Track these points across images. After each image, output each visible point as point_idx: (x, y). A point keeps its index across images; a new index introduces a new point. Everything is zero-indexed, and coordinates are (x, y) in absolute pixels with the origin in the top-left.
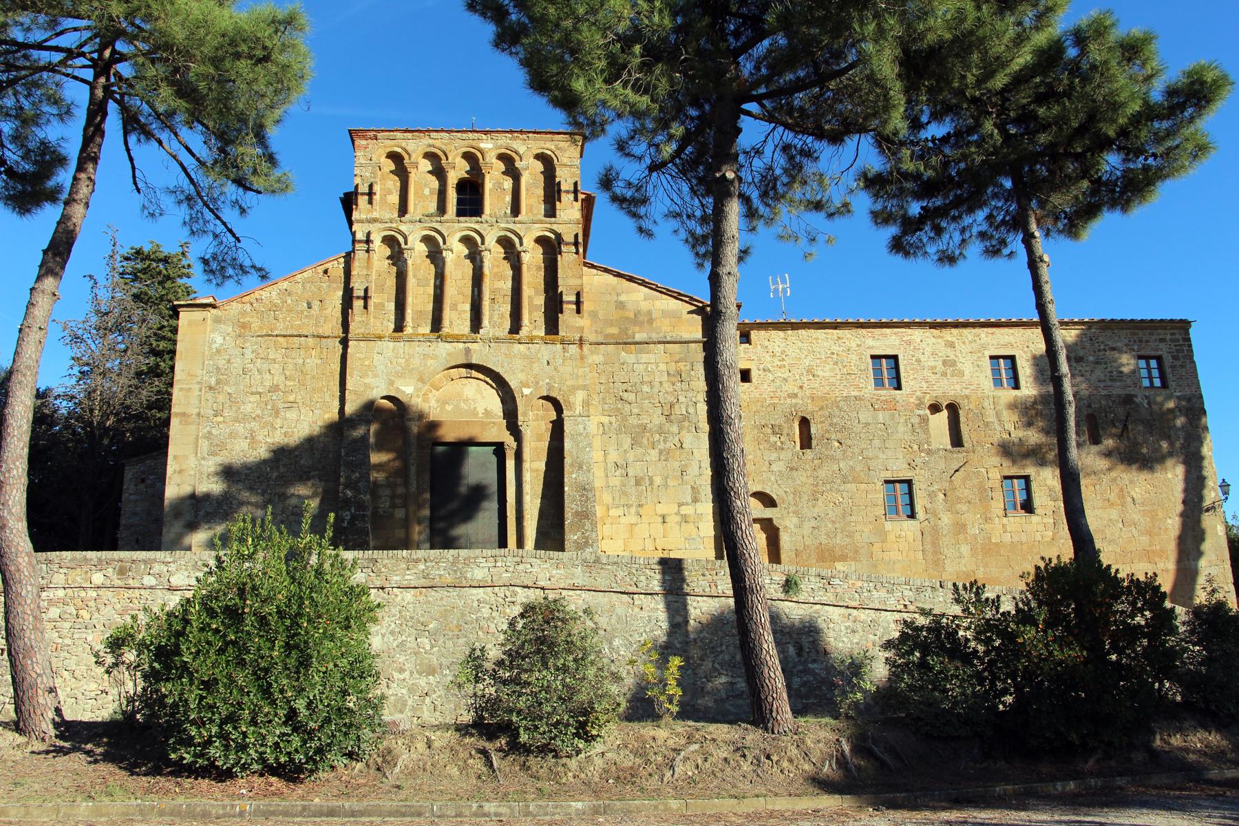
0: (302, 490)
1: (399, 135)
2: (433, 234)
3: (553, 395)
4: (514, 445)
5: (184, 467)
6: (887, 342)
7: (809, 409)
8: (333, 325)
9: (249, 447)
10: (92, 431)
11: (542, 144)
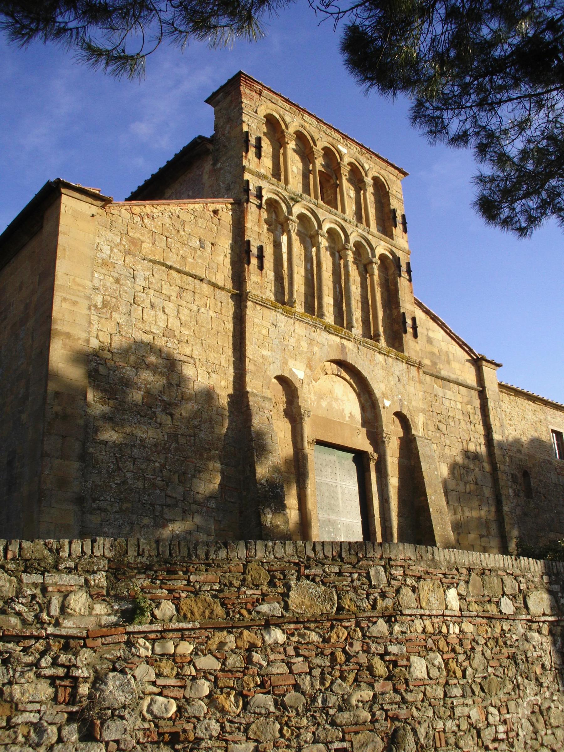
1: (281, 102)
2: (309, 214)
3: (405, 412)
4: (376, 456)
8: (223, 275)
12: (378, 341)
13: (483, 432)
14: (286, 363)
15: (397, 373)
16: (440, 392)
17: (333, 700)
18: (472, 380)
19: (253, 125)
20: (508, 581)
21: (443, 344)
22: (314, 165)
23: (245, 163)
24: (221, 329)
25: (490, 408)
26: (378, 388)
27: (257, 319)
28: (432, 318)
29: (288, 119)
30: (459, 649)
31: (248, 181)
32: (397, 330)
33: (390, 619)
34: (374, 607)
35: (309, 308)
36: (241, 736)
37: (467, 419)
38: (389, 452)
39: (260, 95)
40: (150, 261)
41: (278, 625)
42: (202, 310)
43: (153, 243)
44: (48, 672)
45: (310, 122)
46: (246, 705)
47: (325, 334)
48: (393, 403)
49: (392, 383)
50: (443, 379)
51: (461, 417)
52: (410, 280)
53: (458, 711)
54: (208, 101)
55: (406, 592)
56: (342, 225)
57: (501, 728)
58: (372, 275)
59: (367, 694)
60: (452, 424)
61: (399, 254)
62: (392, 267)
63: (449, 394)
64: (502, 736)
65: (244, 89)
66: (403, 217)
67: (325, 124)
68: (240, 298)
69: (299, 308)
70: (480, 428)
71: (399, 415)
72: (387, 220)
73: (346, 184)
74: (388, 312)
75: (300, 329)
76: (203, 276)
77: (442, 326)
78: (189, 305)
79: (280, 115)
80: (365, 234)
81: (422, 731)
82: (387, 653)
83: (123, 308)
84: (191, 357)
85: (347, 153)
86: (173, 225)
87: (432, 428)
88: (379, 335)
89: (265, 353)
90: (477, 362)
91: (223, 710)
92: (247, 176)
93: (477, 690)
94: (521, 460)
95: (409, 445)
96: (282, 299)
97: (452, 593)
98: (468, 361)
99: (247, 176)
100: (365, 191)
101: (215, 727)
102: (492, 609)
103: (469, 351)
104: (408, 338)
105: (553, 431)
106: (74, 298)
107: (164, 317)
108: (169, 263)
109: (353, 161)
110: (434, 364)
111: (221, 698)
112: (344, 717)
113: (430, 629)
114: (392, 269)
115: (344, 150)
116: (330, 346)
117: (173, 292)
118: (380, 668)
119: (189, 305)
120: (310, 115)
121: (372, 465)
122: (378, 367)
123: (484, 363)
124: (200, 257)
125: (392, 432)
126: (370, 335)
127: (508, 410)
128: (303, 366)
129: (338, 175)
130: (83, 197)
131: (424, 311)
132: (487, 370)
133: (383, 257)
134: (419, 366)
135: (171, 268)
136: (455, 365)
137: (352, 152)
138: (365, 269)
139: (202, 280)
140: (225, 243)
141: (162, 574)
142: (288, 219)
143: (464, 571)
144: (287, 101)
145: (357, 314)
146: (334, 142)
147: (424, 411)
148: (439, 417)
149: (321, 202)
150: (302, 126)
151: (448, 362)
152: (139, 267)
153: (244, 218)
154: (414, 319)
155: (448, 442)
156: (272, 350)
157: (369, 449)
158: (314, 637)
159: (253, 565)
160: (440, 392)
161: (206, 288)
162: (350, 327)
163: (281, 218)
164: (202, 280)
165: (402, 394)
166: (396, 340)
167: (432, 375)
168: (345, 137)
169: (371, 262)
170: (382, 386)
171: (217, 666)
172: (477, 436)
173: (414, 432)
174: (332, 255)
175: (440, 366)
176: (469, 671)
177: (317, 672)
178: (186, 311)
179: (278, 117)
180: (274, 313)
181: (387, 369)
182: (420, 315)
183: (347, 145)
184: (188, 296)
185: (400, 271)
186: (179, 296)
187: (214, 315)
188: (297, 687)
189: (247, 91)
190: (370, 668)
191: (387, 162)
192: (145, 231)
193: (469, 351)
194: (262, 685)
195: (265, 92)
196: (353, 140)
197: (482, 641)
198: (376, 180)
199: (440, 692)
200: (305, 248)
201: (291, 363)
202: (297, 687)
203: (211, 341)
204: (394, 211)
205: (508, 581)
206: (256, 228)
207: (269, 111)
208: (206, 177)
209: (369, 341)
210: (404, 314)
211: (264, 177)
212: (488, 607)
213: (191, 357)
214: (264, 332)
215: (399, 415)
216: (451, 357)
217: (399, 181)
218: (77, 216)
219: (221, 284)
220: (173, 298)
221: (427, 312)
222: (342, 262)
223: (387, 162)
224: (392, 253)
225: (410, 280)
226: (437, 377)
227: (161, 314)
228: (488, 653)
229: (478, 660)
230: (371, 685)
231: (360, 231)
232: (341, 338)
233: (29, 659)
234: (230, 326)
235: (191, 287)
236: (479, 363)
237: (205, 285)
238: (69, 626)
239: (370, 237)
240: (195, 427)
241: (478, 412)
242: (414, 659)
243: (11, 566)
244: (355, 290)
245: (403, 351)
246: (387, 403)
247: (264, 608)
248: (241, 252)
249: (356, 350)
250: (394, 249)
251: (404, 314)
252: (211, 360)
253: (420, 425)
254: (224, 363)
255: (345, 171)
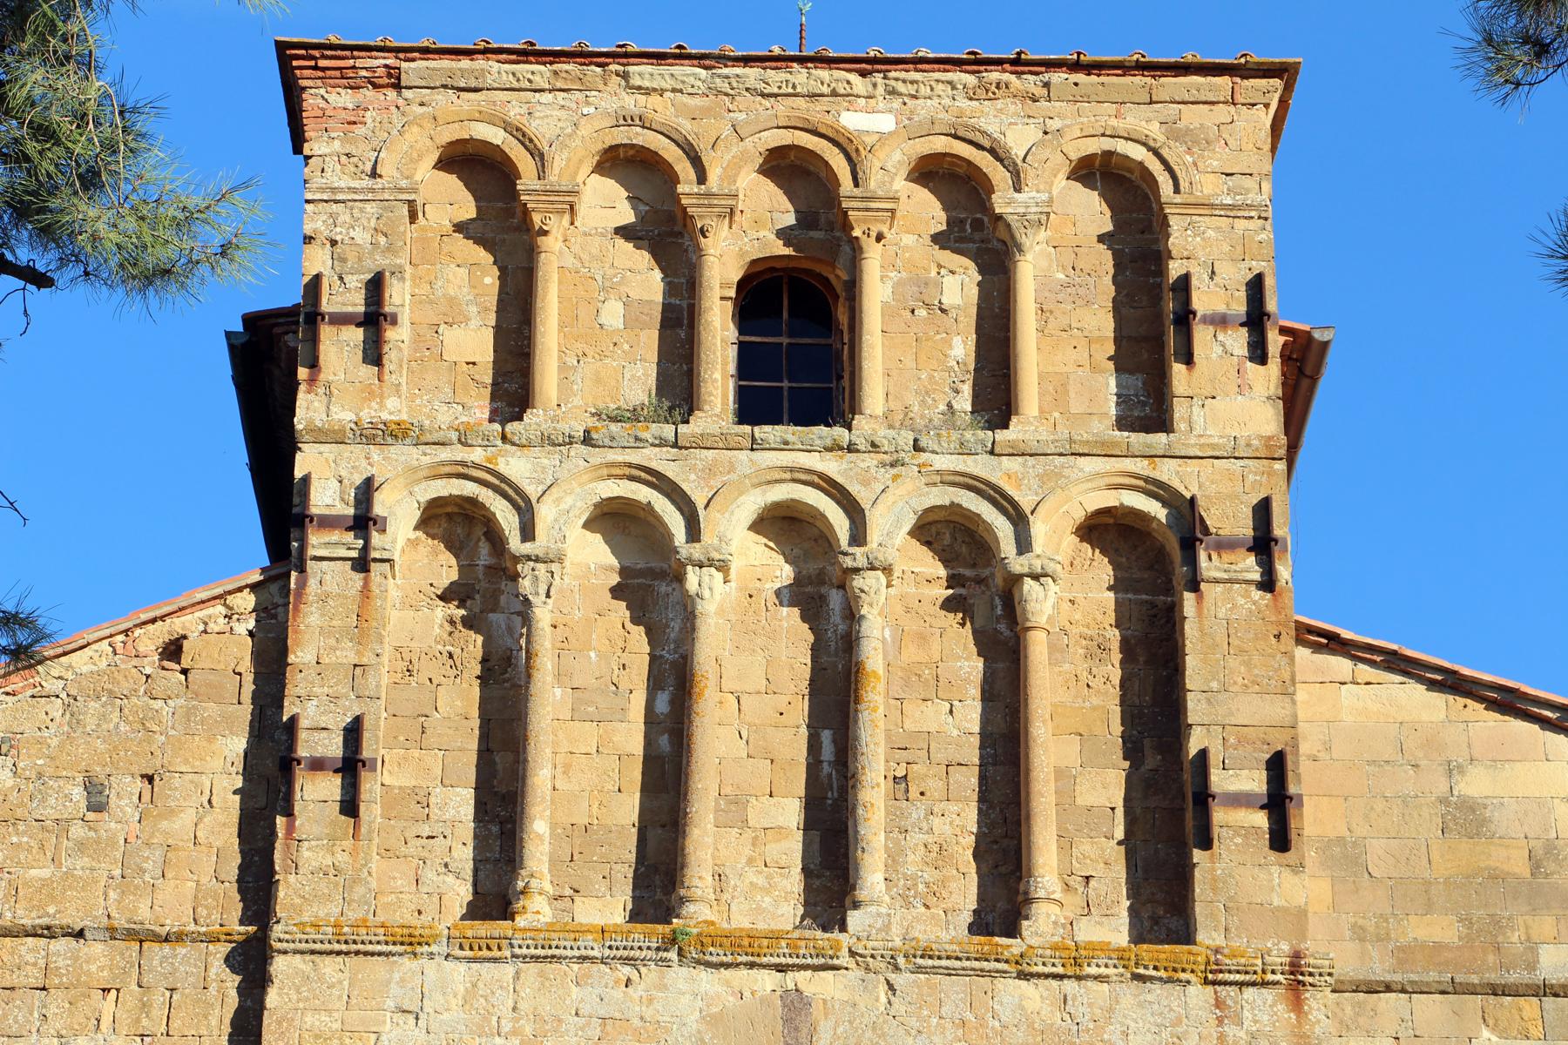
1: (495, 70)
2: (643, 494)
28: (1493, 705)
39: (397, 86)
45: (668, 84)
56: (822, 476)
67: (747, 61)
74: (1152, 761)
79: (508, 127)
131: (1433, 685)
139: (80, 934)
144: (527, 54)
180: (406, 962)
183: (893, 92)
195: (412, 70)
196: (918, 62)
207: (449, 134)
224: (1157, 489)
232: (781, 968)
237: (98, 948)
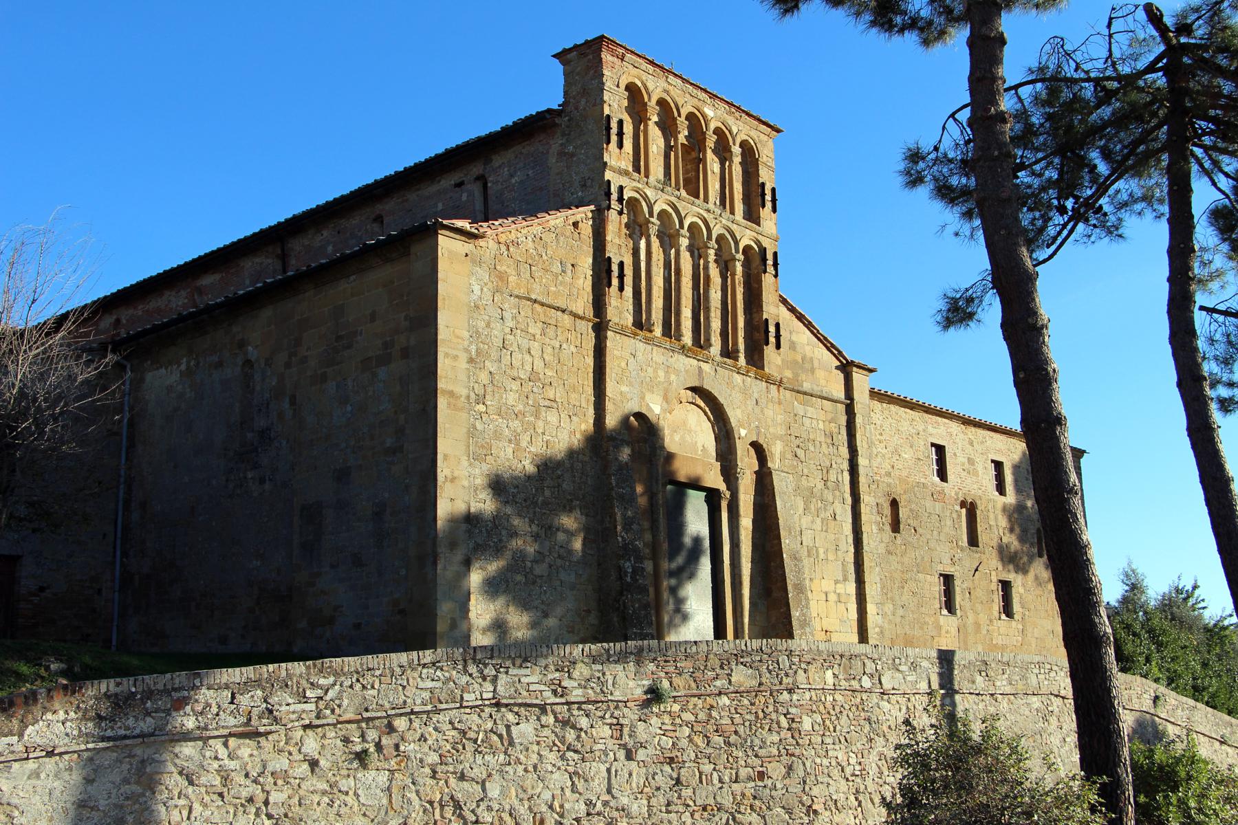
0: (568, 521)
1: (644, 65)
2: (670, 210)
3: (761, 441)
4: (728, 494)
5: (456, 474)
6: (943, 431)
7: (898, 492)
8: (583, 304)
9: (519, 457)
10: (125, 358)
11: (753, 133)
12: (736, 359)
13: (848, 456)
14: (643, 398)
15: (756, 395)
16: (800, 409)
17: (757, 742)
18: (841, 395)
19: (615, 104)
20: (869, 664)
21: (808, 348)
22: (676, 140)
23: (606, 158)
24: (581, 365)
25: (858, 426)
26: (735, 415)
27: (614, 342)
29: (651, 86)
30: (832, 712)
31: (609, 182)
32: (759, 337)
33: (790, 691)
34: (781, 683)
35: (667, 332)
36: (707, 761)
37: (829, 441)
38: (742, 489)
40: (517, 297)
41: (726, 694)
42: (564, 346)
43: (519, 275)
44: (609, 721)
46: (709, 742)
47: (682, 358)
48: (750, 432)
49: (750, 408)
50: (805, 393)
51: (823, 439)
52: (776, 276)
53: (830, 753)
54: (561, 56)
55: (801, 672)
57: (858, 767)
58: (733, 275)
59: (776, 738)
60: (812, 448)
61: (766, 243)
62: (757, 261)
63: (811, 411)
64: (857, 773)
65: (606, 56)
66: (773, 190)
67: (692, 84)
68: (600, 328)
69: (658, 331)
70: (844, 451)
71: (757, 447)
72: (756, 199)
73: (710, 155)
75: (658, 355)
76: (564, 307)
77: (809, 325)
78: (552, 342)
80: (730, 224)
81: (808, 764)
82: (788, 713)
83: (494, 354)
84: (555, 401)
85: (714, 114)
86: (536, 249)
87: (789, 456)
88: (738, 351)
89: (624, 388)
90: (846, 367)
91: (697, 746)
92: (608, 175)
93: (843, 740)
94: (889, 485)
95: (764, 480)
96: (641, 324)
97: (829, 673)
98: (837, 368)
99: (608, 175)
100: (731, 161)
101: (693, 756)
102: (855, 684)
103: (838, 354)
104: (769, 350)
105: (933, 445)
106: (455, 352)
107: (530, 360)
108: (533, 297)
109: (720, 125)
110: (796, 375)
111: (696, 738)
112: (762, 752)
113: (814, 698)
114: (757, 261)
115: (709, 112)
116: (687, 371)
117: (535, 329)
118: (784, 722)
119: (552, 342)
120: (676, 75)
121: (724, 504)
122: (738, 391)
123: (855, 369)
124: (561, 283)
125: (747, 464)
126: (729, 353)
127: (878, 423)
128: (659, 399)
129: (701, 147)
130: (458, 237)
132: (857, 376)
133: (747, 249)
134: (780, 384)
135: (535, 301)
136: (820, 374)
137: (719, 113)
138: (725, 267)
140: (586, 262)
141: (662, 663)
142: (649, 222)
143: (837, 657)
144: (652, 63)
145: (716, 324)
146: (699, 104)
147: (780, 438)
148: (797, 442)
149: (683, 193)
150: (666, 91)
151: (813, 370)
152: (506, 306)
153: (604, 228)
154: (777, 326)
155: (806, 471)
156: (631, 384)
157: (722, 487)
158: (746, 702)
159: (711, 656)
160: (800, 409)
161: (567, 320)
162: (708, 344)
163: (641, 220)
164: (563, 311)
165: (759, 420)
166: (755, 358)
167: (793, 390)
168: (713, 96)
169: (734, 259)
170: (738, 412)
171: (693, 718)
172: (839, 461)
173: (770, 464)
174: (692, 256)
175: (803, 377)
176: (838, 728)
177: (747, 724)
178: (549, 350)
179: (640, 84)
181: (745, 391)
182: (784, 315)
184: (551, 331)
185: (765, 265)
186: (543, 334)
187: (574, 350)
188: (736, 732)
189: (610, 58)
190: (778, 723)
191: (759, 120)
192: (510, 261)
193: (838, 354)
194: (717, 731)
197: (847, 707)
198: (744, 144)
199: (819, 739)
200: (664, 251)
201: (648, 397)
202: (736, 732)
203: (573, 380)
204: (763, 185)
205: (869, 664)
206: (617, 241)
208: (552, 160)
209: (728, 361)
210: (767, 320)
211: (626, 173)
212: (853, 683)
213: (555, 401)
214: (623, 364)
215: (757, 447)
216: (816, 364)
217: (771, 143)
218: (452, 255)
219: (581, 313)
220: (538, 336)
221: (792, 310)
222: (702, 262)
223: (759, 120)
224: (758, 243)
225: (776, 276)
226: (798, 392)
227: (527, 357)
228: (851, 715)
229: (844, 719)
230: (778, 733)
231: (724, 221)
233: (600, 714)
234: (590, 361)
235: (553, 322)
236: (848, 368)
238: (617, 695)
239: (734, 227)
240: (559, 477)
241: (844, 432)
242: (804, 717)
243: (586, 660)
244: (715, 296)
245: (762, 368)
246: (743, 432)
247: (718, 683)
248: (602, 271)
249: (713, 373)
250: (760, 238)
251: (767, 320)
252: (573, 402)
253: (777, 456)
254: (584, 405)
255: (711, 141)
